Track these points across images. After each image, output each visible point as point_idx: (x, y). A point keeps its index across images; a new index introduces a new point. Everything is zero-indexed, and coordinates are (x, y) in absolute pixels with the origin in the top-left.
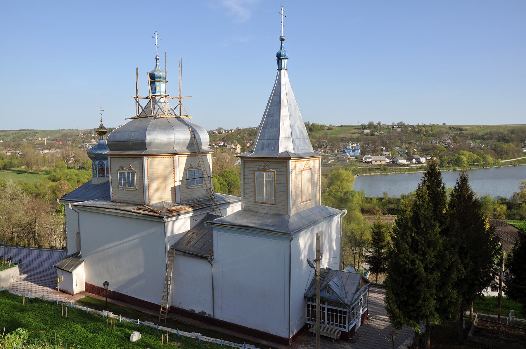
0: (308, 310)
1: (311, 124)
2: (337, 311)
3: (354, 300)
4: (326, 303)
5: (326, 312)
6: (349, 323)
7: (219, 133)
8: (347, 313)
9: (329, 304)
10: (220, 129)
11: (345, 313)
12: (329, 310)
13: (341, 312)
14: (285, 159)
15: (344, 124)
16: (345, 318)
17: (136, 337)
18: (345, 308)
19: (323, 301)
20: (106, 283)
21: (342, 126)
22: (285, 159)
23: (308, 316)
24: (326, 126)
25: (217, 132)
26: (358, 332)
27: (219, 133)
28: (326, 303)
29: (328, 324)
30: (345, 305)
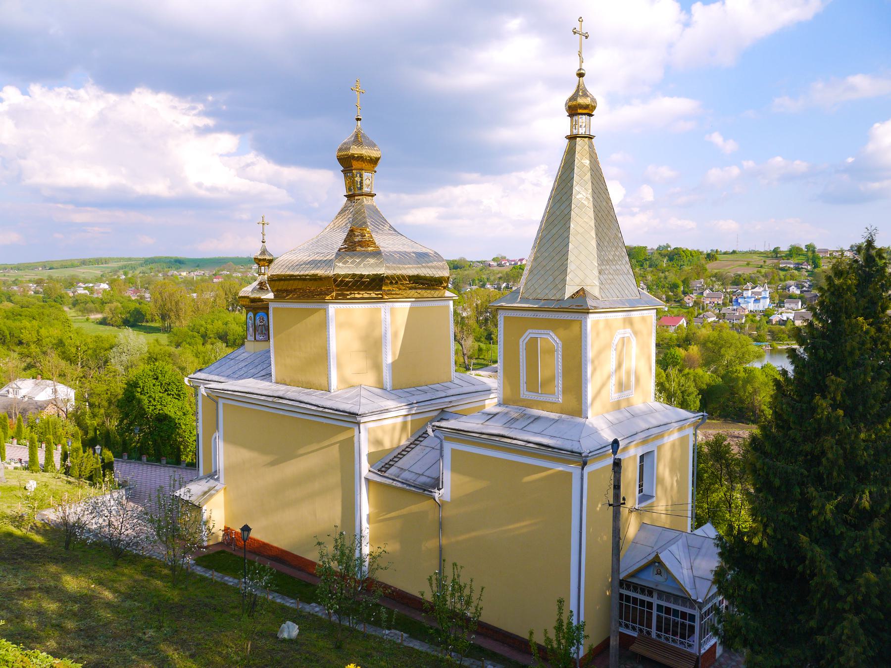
0: (621, 605)
1: (673, 247)
2: (676, 612)
3: (710, 595)
4: (655, 595)
5: (655, 612)
6: (700, 639)
7: (500, 265)
8: (697, 619)
9: (660, 598)
10: (504, 258)
11: (692, 618)
12: (660, 607)
13: (684, 615)
14: (579, 305)
15: (739, 249)
16: (692, 628)
17: (290, 630)
18: (692, 607)
19: (638, 594)
20: (246, 529)
21: (734, 252)
22: (579, 305)
23: (621, 617)
24: (701, 253)
25: (495, 264)
26: (722, 660)
27: (500, 265)
28: (655, 595)
29: (658, 636)
30: (692, 603)
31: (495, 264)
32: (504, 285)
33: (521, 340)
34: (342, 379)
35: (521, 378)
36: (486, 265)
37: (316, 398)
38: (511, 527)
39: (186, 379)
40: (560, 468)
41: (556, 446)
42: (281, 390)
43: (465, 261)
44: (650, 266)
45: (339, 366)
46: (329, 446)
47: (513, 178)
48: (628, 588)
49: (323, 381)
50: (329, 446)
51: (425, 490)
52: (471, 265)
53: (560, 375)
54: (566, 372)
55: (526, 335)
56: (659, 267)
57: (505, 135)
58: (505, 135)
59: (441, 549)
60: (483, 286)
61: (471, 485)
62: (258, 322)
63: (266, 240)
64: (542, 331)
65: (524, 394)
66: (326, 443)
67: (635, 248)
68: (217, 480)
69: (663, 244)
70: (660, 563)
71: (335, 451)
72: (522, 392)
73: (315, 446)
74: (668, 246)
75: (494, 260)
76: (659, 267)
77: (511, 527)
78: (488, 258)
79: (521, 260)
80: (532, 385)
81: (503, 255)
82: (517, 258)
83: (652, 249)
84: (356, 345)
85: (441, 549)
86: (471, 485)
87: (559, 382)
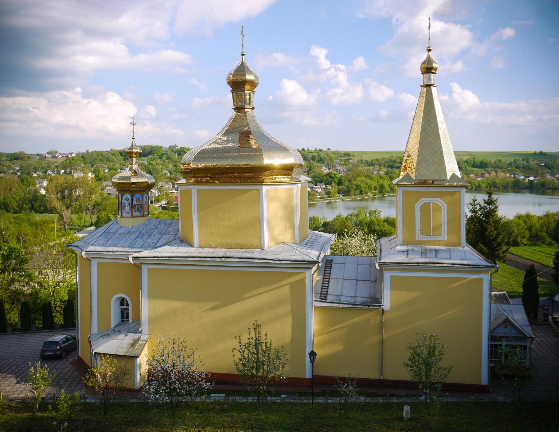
7: (54, 157)
10: (56, 152)
25: (50, 156)
27: (54, 157)
31: (50, 156)
32: (62, 171)
33: (416, 205)
34: (273, 238)
35: (417, 225)
36: (42, 157)
37: (257, 254)
38: (443, 315)
39: (84, 253)
40: (475, 276)
41: (474, 264)
42: (206, 252)
43: (25, 154)
44: (167, 159)
45: (270, 228)
46: (277, 288)
47: (56, 95)
48: (496, 340)
49: (255, 242)
50: (277, 288)
51: (369, 306)
52: (29, 157)
53: (446, 224)
54: (449, 222)
55: (420, 201)
56: (173, 159)
57: (50, 64)
58: (50, 64)
59: (382, 343)
60: (45, 172)
61: (405, 296)
62: (135, 202)
63: (135, 137)
64: (433, 199)
65: (419, 236)
66: (282, 283)
67: (155, 147)
68: (141, 332)
69: (173, 144)
70: (510, 322)
71: (286, 291)
72: (417, 236)
73: (263, 289)
74: (176, 146)
75: (48, 153)
76: (173, 159)
77: (443, 315)
78: (44, 152)
79: (71, 154)
80: (425, 231)
81: (56, 150)
82: (67, 152)
83: (165, 148)
84: (280, 213)
85: (382, 343)
86: (405, 296)
87: (445, 228)
